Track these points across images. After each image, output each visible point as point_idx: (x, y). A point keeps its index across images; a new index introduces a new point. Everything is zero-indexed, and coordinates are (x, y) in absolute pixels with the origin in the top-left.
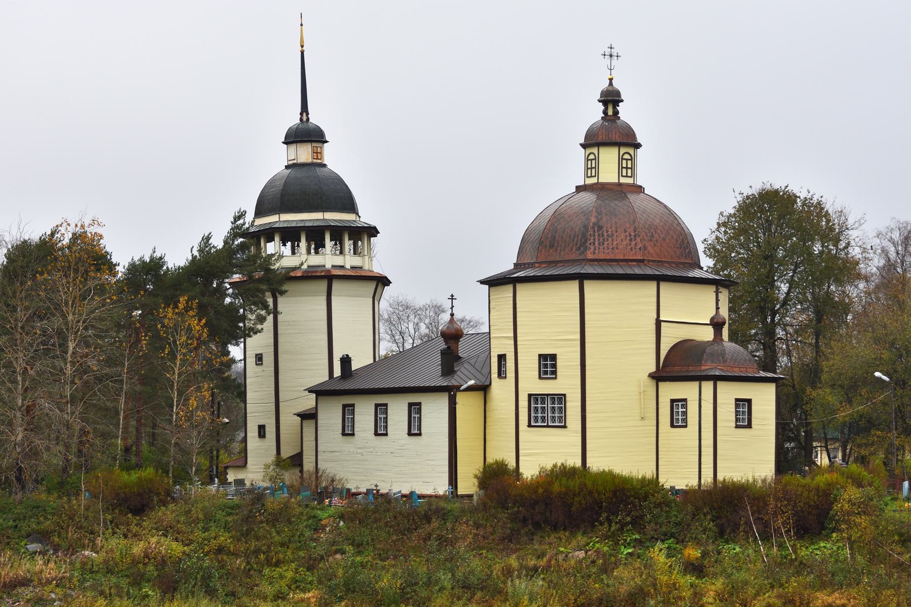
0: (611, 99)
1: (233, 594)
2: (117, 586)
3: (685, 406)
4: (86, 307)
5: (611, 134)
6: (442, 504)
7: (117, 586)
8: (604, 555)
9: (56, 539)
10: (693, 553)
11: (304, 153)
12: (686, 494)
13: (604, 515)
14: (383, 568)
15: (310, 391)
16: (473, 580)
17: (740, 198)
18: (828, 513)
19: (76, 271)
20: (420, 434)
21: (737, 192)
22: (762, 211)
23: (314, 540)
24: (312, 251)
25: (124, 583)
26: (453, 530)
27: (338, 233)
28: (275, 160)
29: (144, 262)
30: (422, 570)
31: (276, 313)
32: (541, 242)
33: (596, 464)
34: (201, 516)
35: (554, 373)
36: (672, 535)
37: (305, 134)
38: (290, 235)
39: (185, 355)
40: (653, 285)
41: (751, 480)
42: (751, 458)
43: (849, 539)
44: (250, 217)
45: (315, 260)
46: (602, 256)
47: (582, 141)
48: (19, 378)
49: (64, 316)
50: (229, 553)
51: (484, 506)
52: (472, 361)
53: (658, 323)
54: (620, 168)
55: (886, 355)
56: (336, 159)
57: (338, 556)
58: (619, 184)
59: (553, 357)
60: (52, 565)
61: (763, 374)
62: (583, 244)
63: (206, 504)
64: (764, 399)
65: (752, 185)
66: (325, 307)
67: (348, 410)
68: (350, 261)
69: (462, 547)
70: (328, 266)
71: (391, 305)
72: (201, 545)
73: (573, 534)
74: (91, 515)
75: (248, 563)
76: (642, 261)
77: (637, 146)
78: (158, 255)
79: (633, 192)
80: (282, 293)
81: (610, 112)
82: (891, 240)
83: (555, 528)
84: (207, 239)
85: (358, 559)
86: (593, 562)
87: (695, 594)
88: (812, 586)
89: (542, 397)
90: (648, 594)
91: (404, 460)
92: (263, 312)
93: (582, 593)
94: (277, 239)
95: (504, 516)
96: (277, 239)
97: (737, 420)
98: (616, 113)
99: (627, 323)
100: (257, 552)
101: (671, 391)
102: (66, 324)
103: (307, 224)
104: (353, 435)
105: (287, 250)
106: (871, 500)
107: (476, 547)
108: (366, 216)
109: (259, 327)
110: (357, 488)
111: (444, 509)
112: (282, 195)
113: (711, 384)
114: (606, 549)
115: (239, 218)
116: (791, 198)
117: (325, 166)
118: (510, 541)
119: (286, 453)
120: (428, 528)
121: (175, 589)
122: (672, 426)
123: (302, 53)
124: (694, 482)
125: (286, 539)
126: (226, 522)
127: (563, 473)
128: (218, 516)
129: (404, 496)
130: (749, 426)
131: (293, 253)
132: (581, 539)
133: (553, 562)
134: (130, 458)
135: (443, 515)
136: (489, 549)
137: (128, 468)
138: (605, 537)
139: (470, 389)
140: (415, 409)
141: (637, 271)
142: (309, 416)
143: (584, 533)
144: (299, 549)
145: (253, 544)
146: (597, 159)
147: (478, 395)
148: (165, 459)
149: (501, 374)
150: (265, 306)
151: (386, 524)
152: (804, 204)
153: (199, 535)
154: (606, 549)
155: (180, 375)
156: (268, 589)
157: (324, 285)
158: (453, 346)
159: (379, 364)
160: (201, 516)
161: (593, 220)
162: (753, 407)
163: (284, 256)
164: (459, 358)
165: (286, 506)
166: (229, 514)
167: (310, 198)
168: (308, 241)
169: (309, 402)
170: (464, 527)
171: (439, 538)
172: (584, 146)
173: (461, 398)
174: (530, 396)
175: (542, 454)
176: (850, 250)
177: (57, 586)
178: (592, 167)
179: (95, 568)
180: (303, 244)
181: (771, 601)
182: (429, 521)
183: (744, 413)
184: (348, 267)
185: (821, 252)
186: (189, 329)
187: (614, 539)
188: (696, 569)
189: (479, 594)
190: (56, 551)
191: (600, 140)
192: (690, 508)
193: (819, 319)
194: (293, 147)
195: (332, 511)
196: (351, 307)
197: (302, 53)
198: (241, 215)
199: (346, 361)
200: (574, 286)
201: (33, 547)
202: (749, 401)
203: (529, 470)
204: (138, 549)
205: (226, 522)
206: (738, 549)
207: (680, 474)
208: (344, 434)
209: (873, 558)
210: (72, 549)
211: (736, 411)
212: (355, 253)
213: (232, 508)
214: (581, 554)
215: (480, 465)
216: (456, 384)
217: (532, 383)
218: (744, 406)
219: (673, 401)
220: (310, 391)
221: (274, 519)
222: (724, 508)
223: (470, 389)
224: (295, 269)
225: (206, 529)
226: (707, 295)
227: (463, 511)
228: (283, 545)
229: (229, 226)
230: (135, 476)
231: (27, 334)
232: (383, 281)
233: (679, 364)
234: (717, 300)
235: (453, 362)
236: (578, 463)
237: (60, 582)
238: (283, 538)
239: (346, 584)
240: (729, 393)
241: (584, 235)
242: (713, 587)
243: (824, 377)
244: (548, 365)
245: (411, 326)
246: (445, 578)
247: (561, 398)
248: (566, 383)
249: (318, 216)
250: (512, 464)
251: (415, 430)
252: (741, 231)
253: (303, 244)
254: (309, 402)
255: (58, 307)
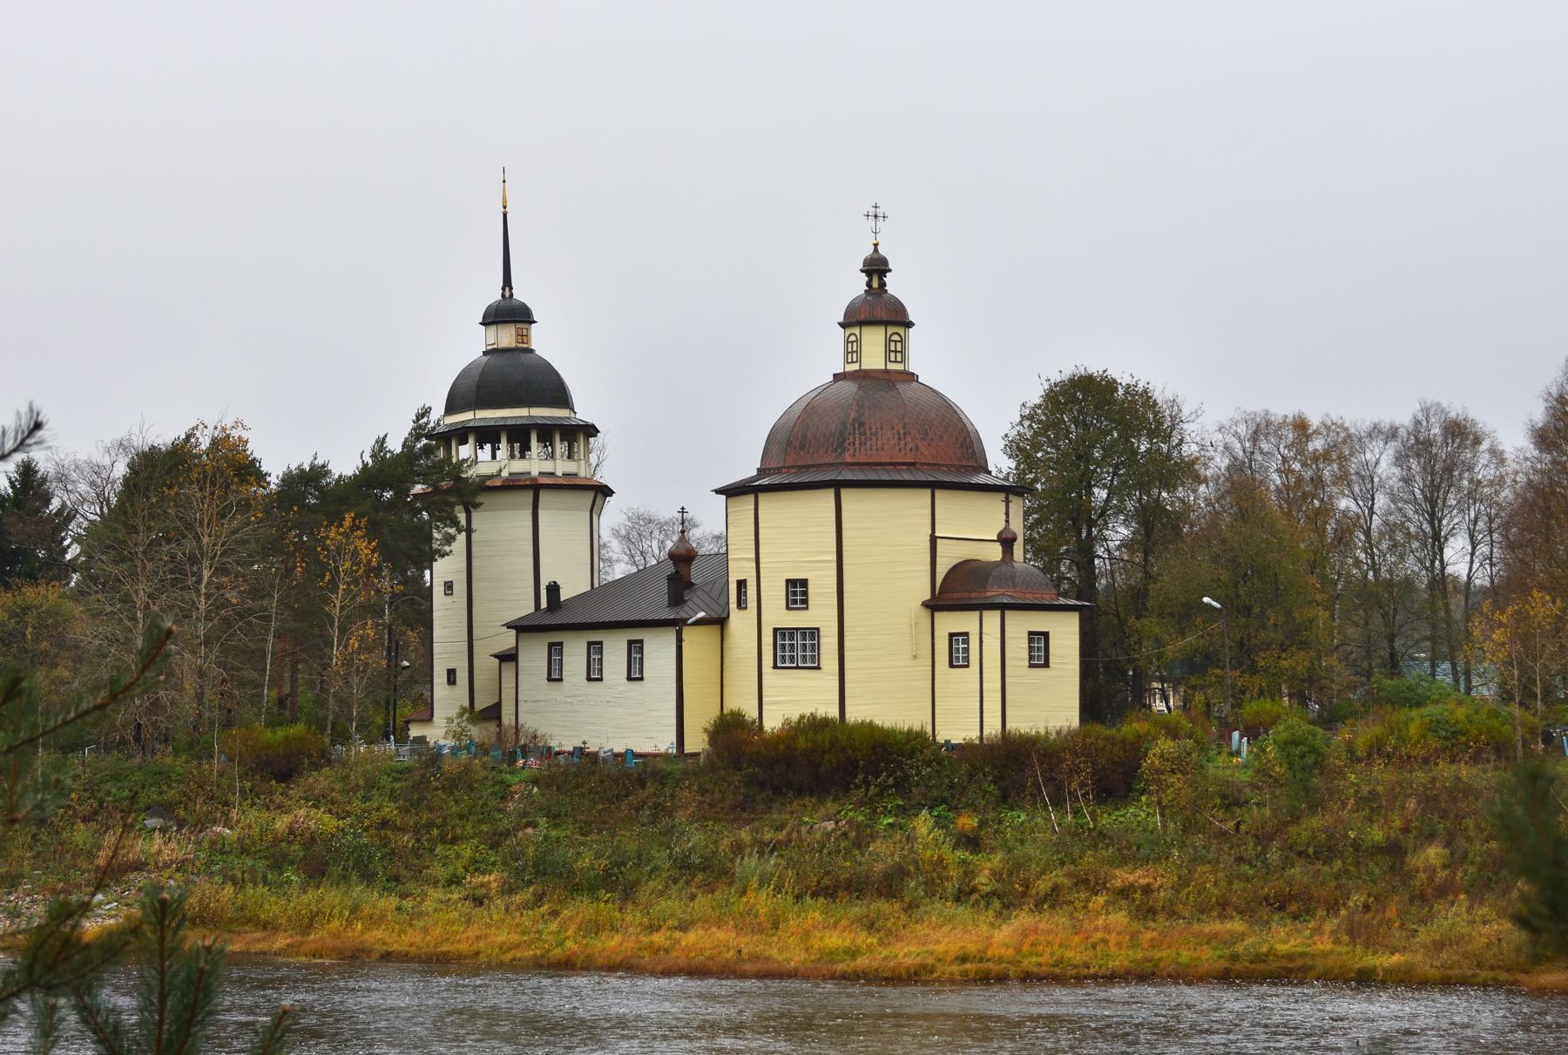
0: (876, 268)
1: (397, 879)
2: (253, 870)
3: (966, 642)
4: (229, 525)
5: (878, 310)
6: (661, 765)
7: (253, 870)
8: (858, 826)
9: (182, 813)
10: (968, 822)
11: (506, 337)
12: (964, 750)
13: (861, 777)
14: (584, 844)
15: (509, 626)
16: (696, 859)
17: (1046, 386)
18: (1139, 766)
19: (213, 483)
20: (641, 679)
21: (1044, 378)
22: (1075, 400)
23: (500, 811)
24: (517, 453)
25: (261, 866)
26: (673, 797)
27: (547, 433)
28: (470, 344)
29: (303, 471)
30: (631, 847)
31: (469, 531)
32: (789, 443)
33: (855, 714)
34: (361, 783)
35: (805, 602)
36: (944, 801)
37: (509, 313)
38: (487, 435)
39: (349, 584)
40: (927, 493)
41: (1042, 731)
42: (1050, 703)
43: (1159, 803)
44: (438, 411)
45: (519, 466)
46: (863, 459)
47: (841, 319)
48: (139, 615)
49: (198, 539)
50: (396, 828)
51: (712, 767)
52: (707, 589)
53: (934, 539)
54: (888, 351)
55: (1225, 576)
56: (545, 342)
57: (530, 831)
58: (886, 371)
59: (804, 583)
60: (173, 845)
61: (1062, 601)
62: (840, 444)
63: (369, 767)
64: (1065, 633)
65: (1061, 368)
66: (530, 524)
67: (555, 649)
68: (562, 467)
69: (680, 817)
70: (535, 473)
71: (629, 519)
72: (360, 819)
73: (821, 800)
74: (224, 781)
75: (418, 840)
76: (913, 464)
77: (909, 325)
78: (320, 462)
79: (903, 381)
80: (477, 506)
81: (875, 284)
82: (1236, 434)
83: (799, 793)
84: (381, 442)
85: (554, 833)
86: (845, 834)
87: (965, 873)
88: (1111, 863)
89: (791, 632)
90: (908, 874)
91: (625, 710)
92: (452, 531)
93: (827, 873)
94: (471, 440)
95: (736, 778)
96: (471, 440)
97: (1031, 658)
98: (882, 285)
99: (895, 541)
100: (429, 826)
101: (950, 622)
102: (200, 548)
103: (509, 422)
104: (561, 680)
105: (485, 453)
106: (1189, 754)
107: (701, 818)
108: (584, 411)
109: (447, 549)
110: (560, 745)
111: (661, 771)
112: (479, 387)
113: (997, 614)
114: (861, 818)
115: (423, 415)
116: (1111, 385)
117: (532, 351)
118: (743, 809)
119: (482, 703)
120: (642, 795)
121: (323, 873)
122: (951, 665)
123: (505, 215)
124: (974, 734)
125: (466, 810)
126: (392, 790)
127: (815, 725)
128: (383, 783)
129: (616, 755)
130: (1046, 665)
131: (494, 457)
132: (831, 806)
133: (795, 835)
134: (285, 709)
135: (661, 778)
136: (717, 820)
137: (272, 724)
138: (861, 804)
139: (699, 622)
140: (635, 647)
141: (907, 477)
142: (508, 657)
143: (834, 800)
144: (482, 821)
145: (425, 816)
146: (859, 341)
147: (715, 629)
148: (321, 713)
149: (741, 604)
150: (455, 523)
151: (590, 791)
152: (1126, 392)
153: (357, 805)
154: (861, 818)
155: (342, 608)
156: (439, 871)
157: (528, 497)
158: (683, 570)
159: (600, 592)
160: (361, 783)
161: (853, 414)
162: (1052, 642)
163: (483, 461)
164: (690, 585)
165: (468, 769)
166: (396, 780)
167: (514, 389)
168: (510, 441)
169: (508, 640)
170: (686, 793)
171: (656, 806)
172: (843, 325)
173: (687, 633)
174: (775, 630)
175: (791, 700)
176: (1185, 448)
177: (178, 870)
178: (853, 350)
179: (227, 848)
180: (503, 445)
181: (1059, 881)
182: (643, 787)
183: (1040, 650)
184: (559, 473)
185: (1148, 451)
186: (356, 552)
187: (870, 804)
188: (972, 842)
189: (700, 876)
190: (180, 827)
191: (862, 317)
192: (965, 767)
193: (1148, 534)
194: (493, 329)
195: (526, 773)
196: (562, 526)
197: (505, 215)
198: (425, 412)
199: (554, 589)
200: (829, 494)
201: (153, 822)
202: (1046, 635)
203: (773, 722)
204: (282, 823)
205: (392, 790)
206: (1023, 817)
207: (958, 726)
208: (550, 679)
209: (1189, 828)
210: (201, 824)
211: (1031, 649)
212: (569, 457)
213: (401, 772)
214: (830, 825)
215: (717, 712)
216: (684, 616)
217: (778, 614)
218: (1039, 643)
219: (951, 635)
220: (509, 626)
221: (452, 785)
222: (1010, 765)
223: (699, 622)
224: (491, 477)
225: (366, 799)
226: (995, 504)
227: (686, 773)
228: (461, 817)
229: (411, 425)
230: (281, 733)
231: (151, 560)
232: (605, 491)
233: (959, 590)
234: (1007, 514)
235: (684, 589)
236: (833, 712)
237: (181, 866)
238: (463, 808)
239: (535, 865)
240: (1021, 625)
241: (841, 434)
242: (988, 865)
243: (1150, 603)
244: (797, 592)
245: (655, 544)
246: (661, 856)
247: (814, 633)
248: (820, 614)
249: (522, 412)
250: (751, 713)
251: (635, 673)
252: (1045, 427)
253: (503, 445)
254: (508, 640)
255: (190, 526)
